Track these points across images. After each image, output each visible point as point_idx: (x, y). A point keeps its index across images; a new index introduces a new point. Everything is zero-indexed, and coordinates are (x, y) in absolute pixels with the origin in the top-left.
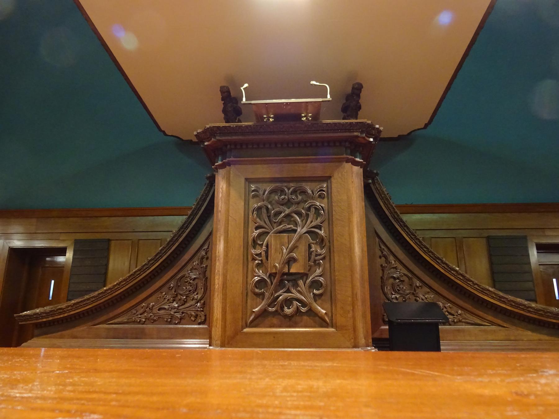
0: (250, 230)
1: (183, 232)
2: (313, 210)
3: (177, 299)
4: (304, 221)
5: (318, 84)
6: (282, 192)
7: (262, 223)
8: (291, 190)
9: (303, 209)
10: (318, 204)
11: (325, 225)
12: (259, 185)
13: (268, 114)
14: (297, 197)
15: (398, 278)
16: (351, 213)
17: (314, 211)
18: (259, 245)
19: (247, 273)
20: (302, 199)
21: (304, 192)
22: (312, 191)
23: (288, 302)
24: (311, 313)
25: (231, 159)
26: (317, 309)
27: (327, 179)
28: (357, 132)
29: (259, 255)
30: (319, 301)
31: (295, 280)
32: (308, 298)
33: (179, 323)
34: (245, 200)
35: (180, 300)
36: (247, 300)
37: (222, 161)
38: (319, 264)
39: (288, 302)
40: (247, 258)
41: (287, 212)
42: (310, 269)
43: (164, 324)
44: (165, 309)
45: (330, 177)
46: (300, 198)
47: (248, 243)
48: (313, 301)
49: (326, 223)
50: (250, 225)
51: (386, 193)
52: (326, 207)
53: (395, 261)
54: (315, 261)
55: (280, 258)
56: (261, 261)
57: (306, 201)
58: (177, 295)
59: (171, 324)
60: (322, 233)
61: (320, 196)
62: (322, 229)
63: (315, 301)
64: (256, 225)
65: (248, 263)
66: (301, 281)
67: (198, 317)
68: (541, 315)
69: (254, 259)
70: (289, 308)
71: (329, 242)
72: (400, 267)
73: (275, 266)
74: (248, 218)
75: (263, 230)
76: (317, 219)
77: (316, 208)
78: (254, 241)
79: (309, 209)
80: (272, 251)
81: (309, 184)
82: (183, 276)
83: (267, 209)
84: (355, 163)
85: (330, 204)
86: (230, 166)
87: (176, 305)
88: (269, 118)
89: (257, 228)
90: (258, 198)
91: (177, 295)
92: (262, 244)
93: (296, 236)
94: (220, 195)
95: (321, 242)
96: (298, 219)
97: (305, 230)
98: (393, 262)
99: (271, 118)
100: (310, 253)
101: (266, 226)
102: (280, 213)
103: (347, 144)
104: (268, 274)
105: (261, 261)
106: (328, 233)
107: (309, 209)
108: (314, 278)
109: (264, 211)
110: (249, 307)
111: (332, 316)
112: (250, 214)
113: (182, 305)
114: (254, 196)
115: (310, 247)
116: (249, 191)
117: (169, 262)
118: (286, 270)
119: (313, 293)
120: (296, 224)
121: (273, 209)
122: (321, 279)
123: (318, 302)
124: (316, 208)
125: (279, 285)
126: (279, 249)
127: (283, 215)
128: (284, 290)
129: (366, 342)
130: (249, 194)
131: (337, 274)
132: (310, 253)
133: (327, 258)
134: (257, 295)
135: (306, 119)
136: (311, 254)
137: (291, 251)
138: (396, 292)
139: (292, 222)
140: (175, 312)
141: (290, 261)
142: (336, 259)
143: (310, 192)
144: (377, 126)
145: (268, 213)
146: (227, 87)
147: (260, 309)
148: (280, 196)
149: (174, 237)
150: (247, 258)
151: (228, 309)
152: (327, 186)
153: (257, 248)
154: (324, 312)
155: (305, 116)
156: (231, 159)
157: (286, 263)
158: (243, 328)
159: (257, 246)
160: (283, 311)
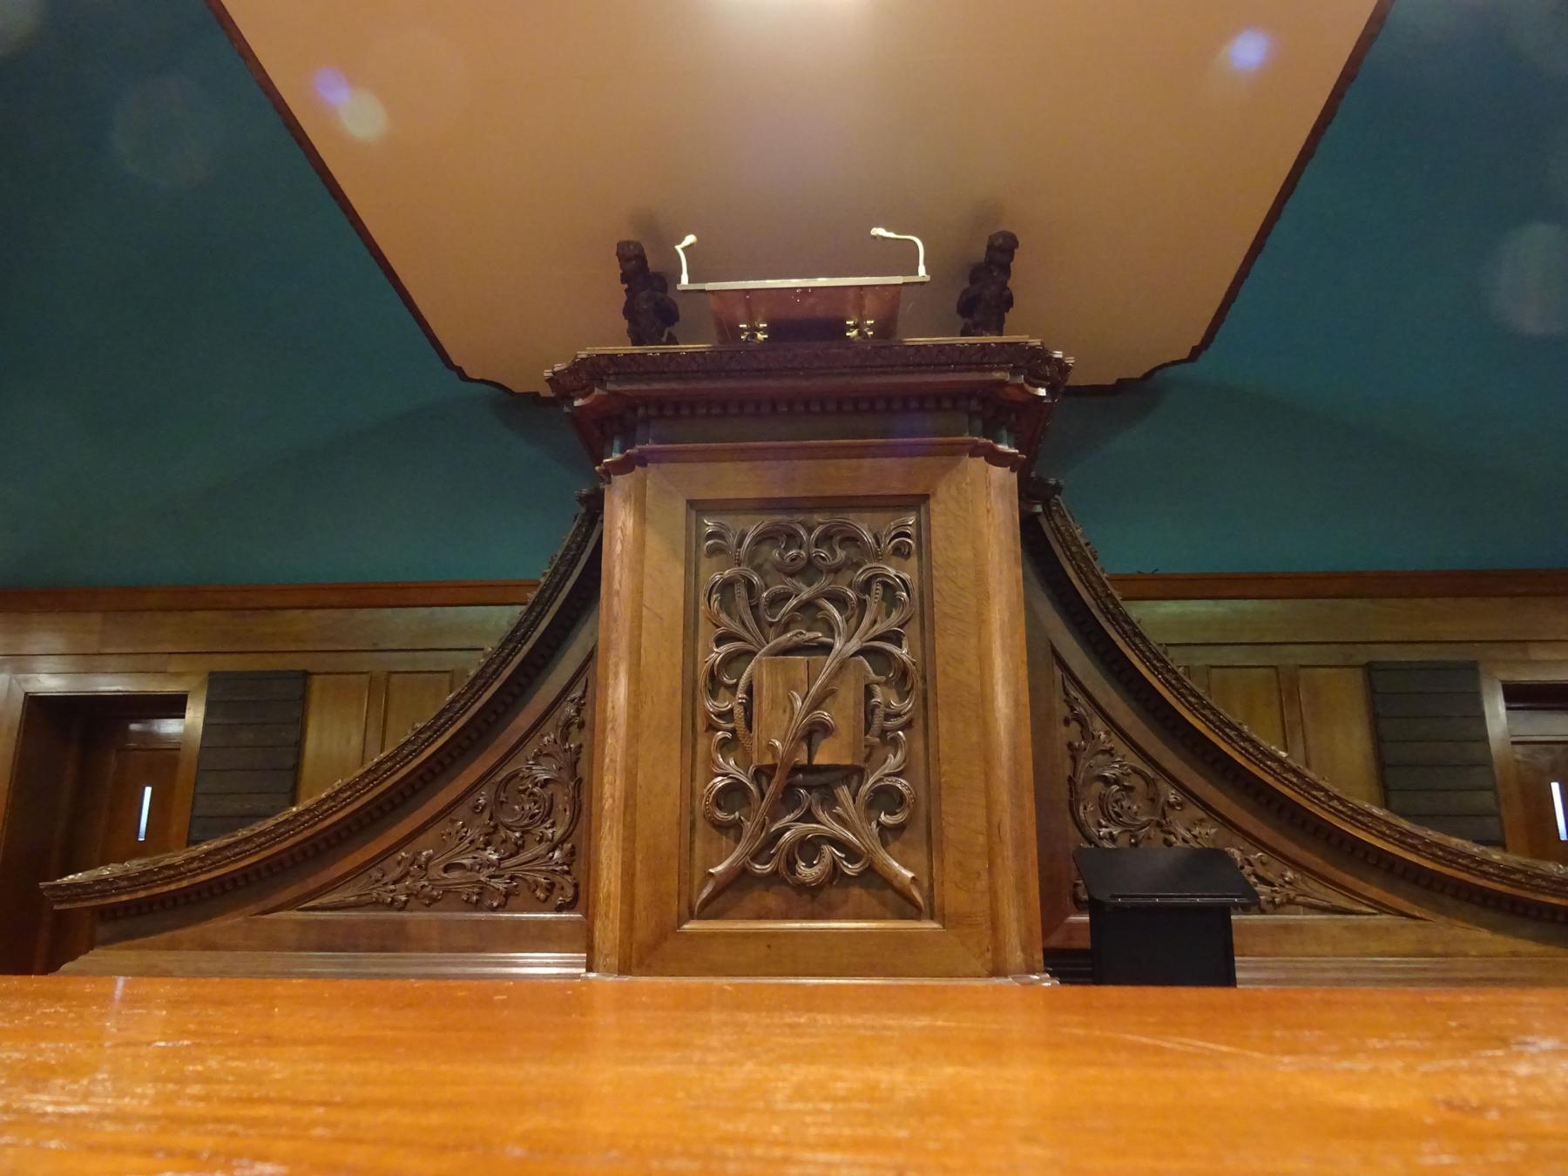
0: (700, 646)
1: (514, 652)
2: (877, 588)
3: (497, 838)
4: (853, 621)
5: (891, 235)
6: (792, 538)
7: (735, 627)
8: (817, 532)
9: (850, 586)
10: (892, 572)
11: (912, 631)
12: (728, 520)
13: (751, 319)
14: (833, 552)
15: (1116, 782)
16: (984, 597)
17: (880, 592)
18: (728, 687)
19: (693, 766)
20: (847, 558)
21: (852, 539)
22: (875, 537)
23: (808, 848)
24: (873, 877)
25: (647, 446)
26: (889, 866)
27: (918, 501)
28: (1001, 369)
29: (728, 715)
30: (896, 846)
31: (826, 786)
32: (863, 836)
33: (502, 907)
34: (687, 562)
35: (504, 841)
36: (692, 843)
37: (622, 451)
38: (895, 742)
39: (808, 848)
40: (694, 725)
41: (804, 596)
42: (871, 756)
43: (460, 910)
44: (462, 866)
45: (925, 498)
46: (841, 554)
47: (695, 681)
48: (877, 844)
49: (915, 626)
50: (702, 632)
51: (1083, 541)
52: (916, 580)
53: (1107, 733)
54: (884, 732)
55: (786, 724)
56: (733, 731)
57: (858, 565)
58: (496, 827)
59: (481, 910)
60: (903, 653)
61: (897, 550)
62: (905, 642)
63: (885, 844)
64: (719, 631)
65: (695, 739)
66: (845, 788)
67: (556, 891)
68: (1518, 884)
69: (712, 728)
70: (810, 865)
71: (924, 678)
72: (1122, 749)
73: (772, 748)
74: (697, 611)
75: (738, 644)
76: (888, 615)
77: (885, 585)
78: (713, 677)
79: (866, 587)
80: (763, 706)
81: (867, 515)
82: (514, 775)
83: (750, 586)
84: (997, 459)
85: (926, 572)
86: (644, 465)
87: (495, 857)
88: (754, 330)
89: (720, 641)
90: (723, 556)
91: (496, 827)
92: (736, 685)
93: (830, 663)
94: (618, 548)
95: (901, 678)
96: (837, 614)
97: (854, 645)
98: (1103, 736)
99: (759, 330)
100: (870, 711)
101: (747, 636)
102: (786, 597)
103: (974, 403)
104: (752, 769)
105: (733, 731)
106: (919, 653)
107: (866, 587)
108: (880, 780)
109: (741, 591)
110: (698, 863)
111: (931, 886)
112: (703, 599)
113: (511, 856)
114: (712, 551)
115: (869, 693)
116: (698, 536)
117: (474, 735)
118: (802, 758)
119: (879, 824)
120: (830, 629)
121: (767, 587)
122: (901, 784)
123: (891, 848)
124: (885, 585)
125: (783, 801)
126: (782, 699)
127: (793, 602)
128: (798, 813)
129: (1026, 961)
130: (698, 546)
131: (944, 768)
132: (870, 711)
133: (919, 725)
134: (721, 827)
135: (860, 333)
136: (872, 712)
137: (817, 704)
138: (1110, 819)
139: (820, 624)
140: (491, 877)
141: (814, 732)
142: (943, 726)
143: (868, 538)
144: (1058, 354)
145: (750, 597)
146: (638, 245)
147: (730, 867)
148: (787, 549)
149: (487, 665)
150: (693, 725)
151: (638, 866)
152: (918, 522)
153: (721, 696)
154: (910, 875)
155: (855, 327)
156: (647, 446)
157: (803, 738)
158: (681, 921)
159: (722, 690)
160: (794, 872)
